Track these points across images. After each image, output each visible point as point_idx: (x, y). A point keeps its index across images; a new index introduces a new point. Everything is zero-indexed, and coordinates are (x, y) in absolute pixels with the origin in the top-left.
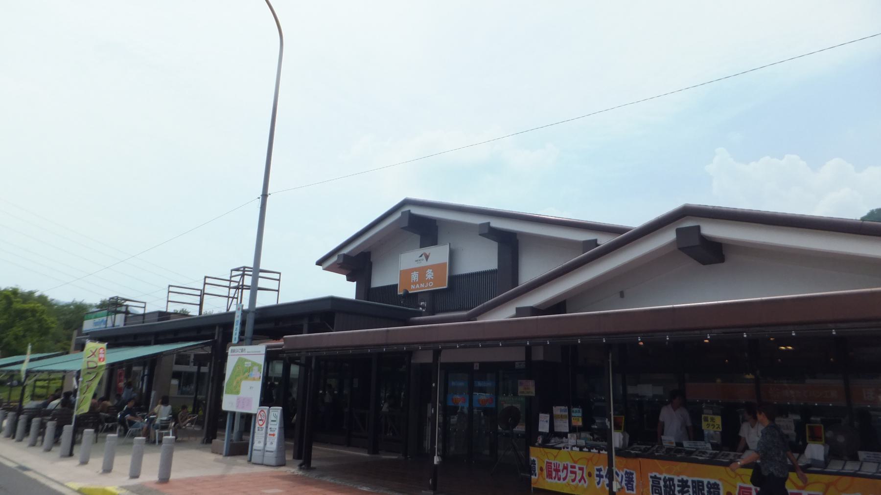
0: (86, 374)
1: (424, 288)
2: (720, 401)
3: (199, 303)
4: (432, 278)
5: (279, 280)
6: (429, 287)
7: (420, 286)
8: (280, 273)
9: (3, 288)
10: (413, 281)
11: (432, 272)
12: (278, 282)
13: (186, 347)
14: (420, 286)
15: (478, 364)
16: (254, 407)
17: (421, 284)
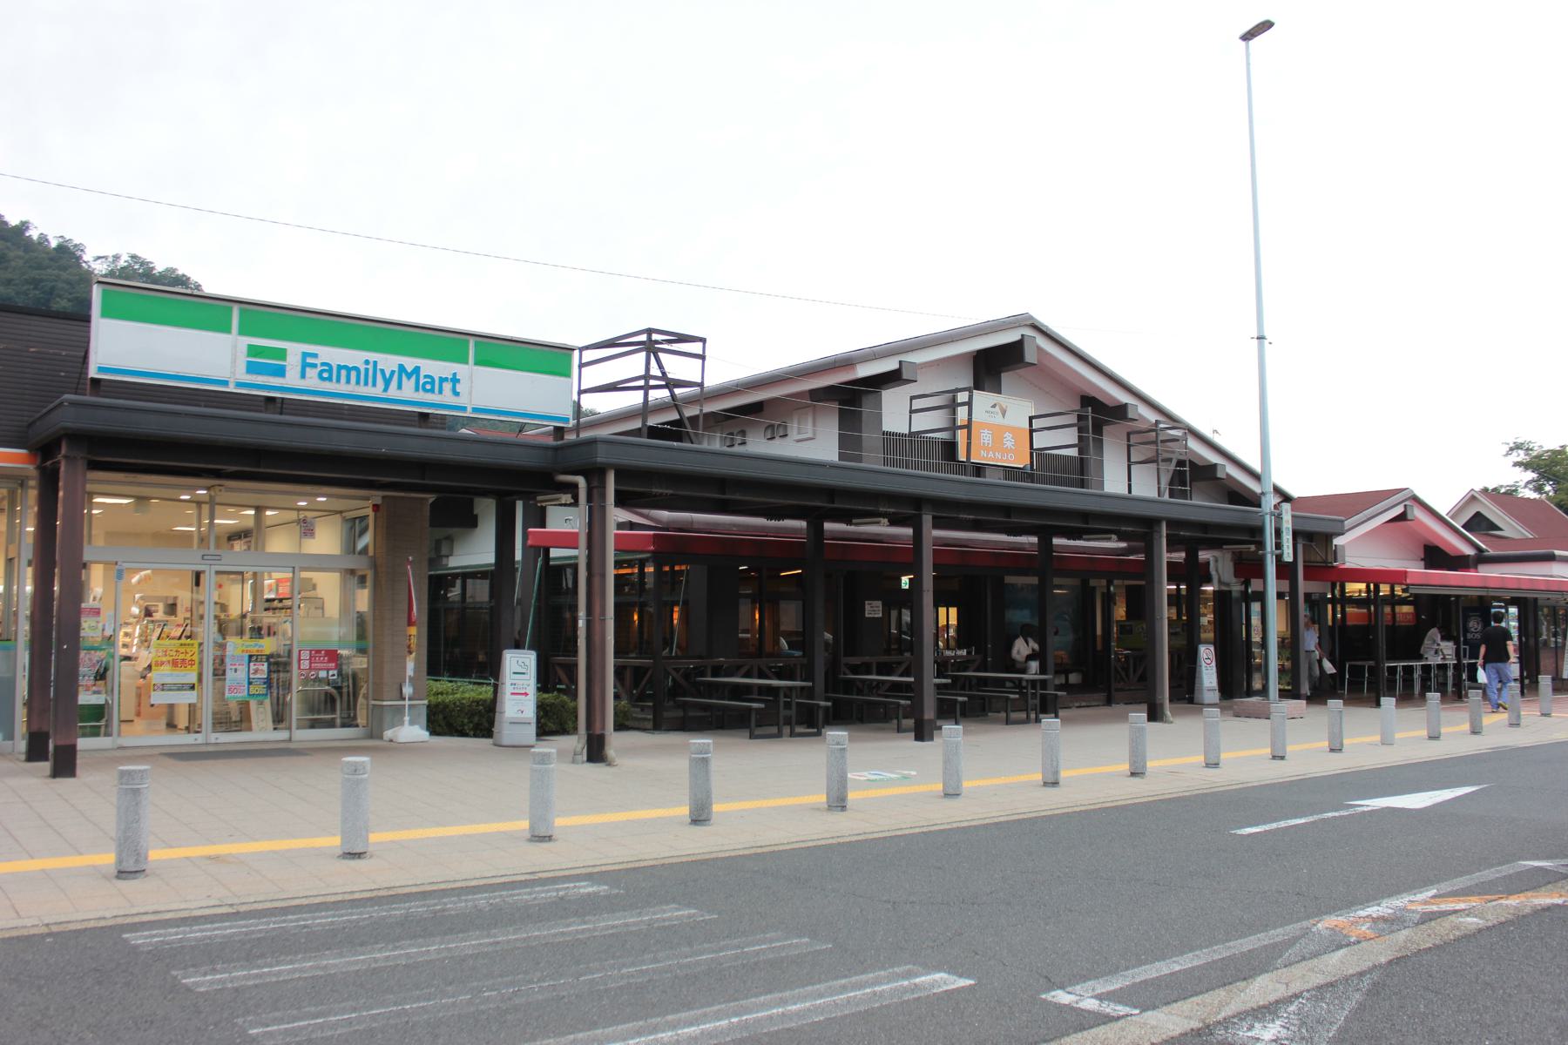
0: (1026, 325)
1: (1001, 460)
2: (1371, 637)
3: (209, 742)
4: (1013, 448)
5: (702, 357)
6: (1007, 461)
7: (987, 455)
8: (703, 340)
9: (13, 220)
10: (984, 443)
11: (1012, 438)
12: (700, 361)
13: (380, 423)
14: (987, 455)
15: (1261, 589)
16: (1314, 649)
17: (997, 454)
